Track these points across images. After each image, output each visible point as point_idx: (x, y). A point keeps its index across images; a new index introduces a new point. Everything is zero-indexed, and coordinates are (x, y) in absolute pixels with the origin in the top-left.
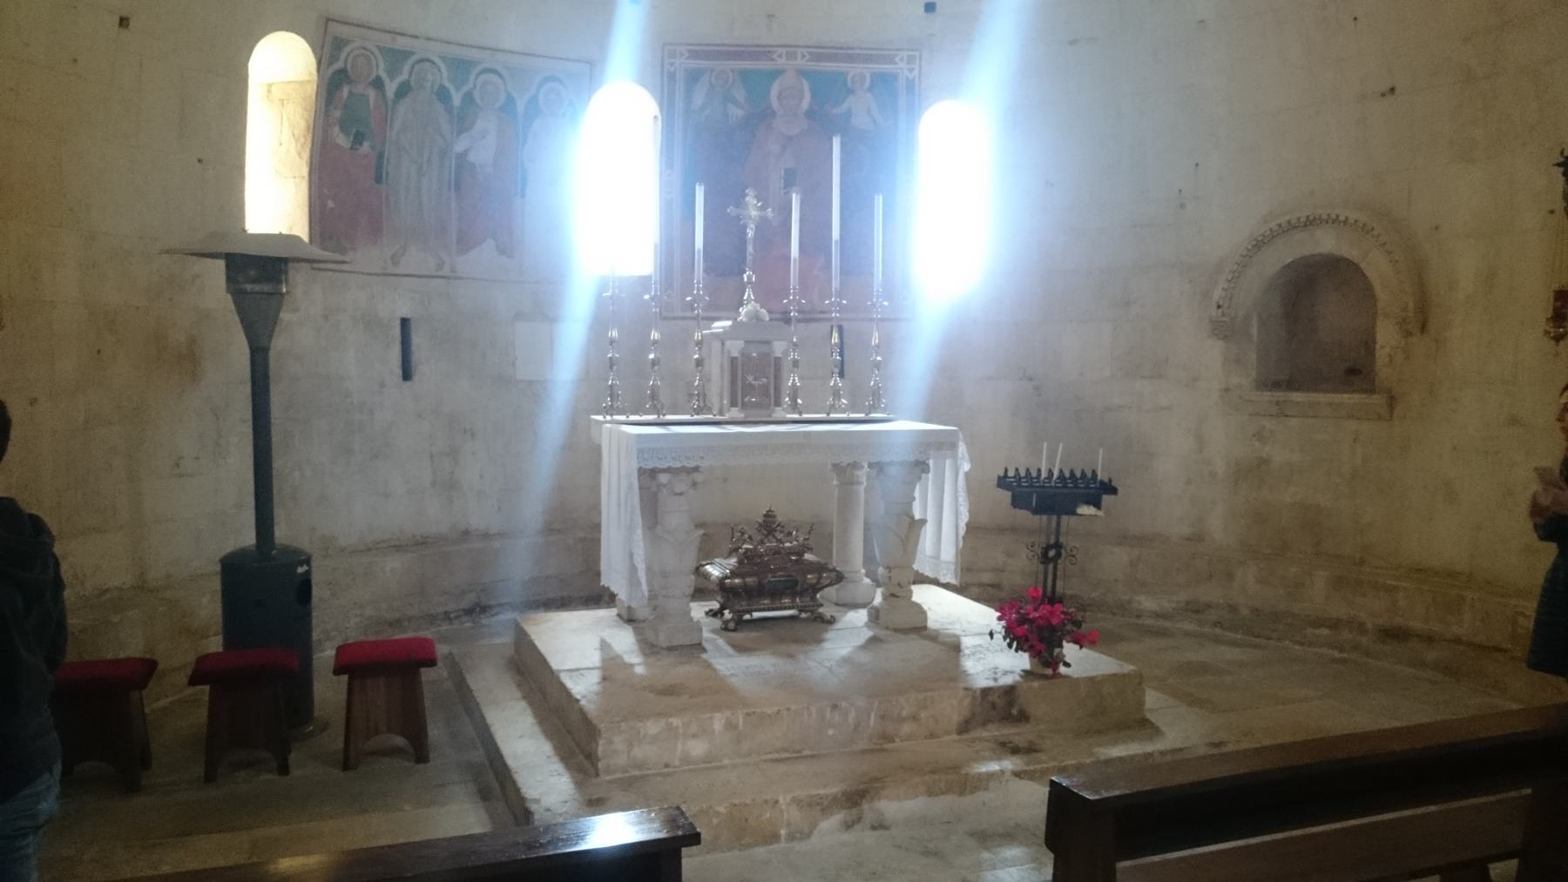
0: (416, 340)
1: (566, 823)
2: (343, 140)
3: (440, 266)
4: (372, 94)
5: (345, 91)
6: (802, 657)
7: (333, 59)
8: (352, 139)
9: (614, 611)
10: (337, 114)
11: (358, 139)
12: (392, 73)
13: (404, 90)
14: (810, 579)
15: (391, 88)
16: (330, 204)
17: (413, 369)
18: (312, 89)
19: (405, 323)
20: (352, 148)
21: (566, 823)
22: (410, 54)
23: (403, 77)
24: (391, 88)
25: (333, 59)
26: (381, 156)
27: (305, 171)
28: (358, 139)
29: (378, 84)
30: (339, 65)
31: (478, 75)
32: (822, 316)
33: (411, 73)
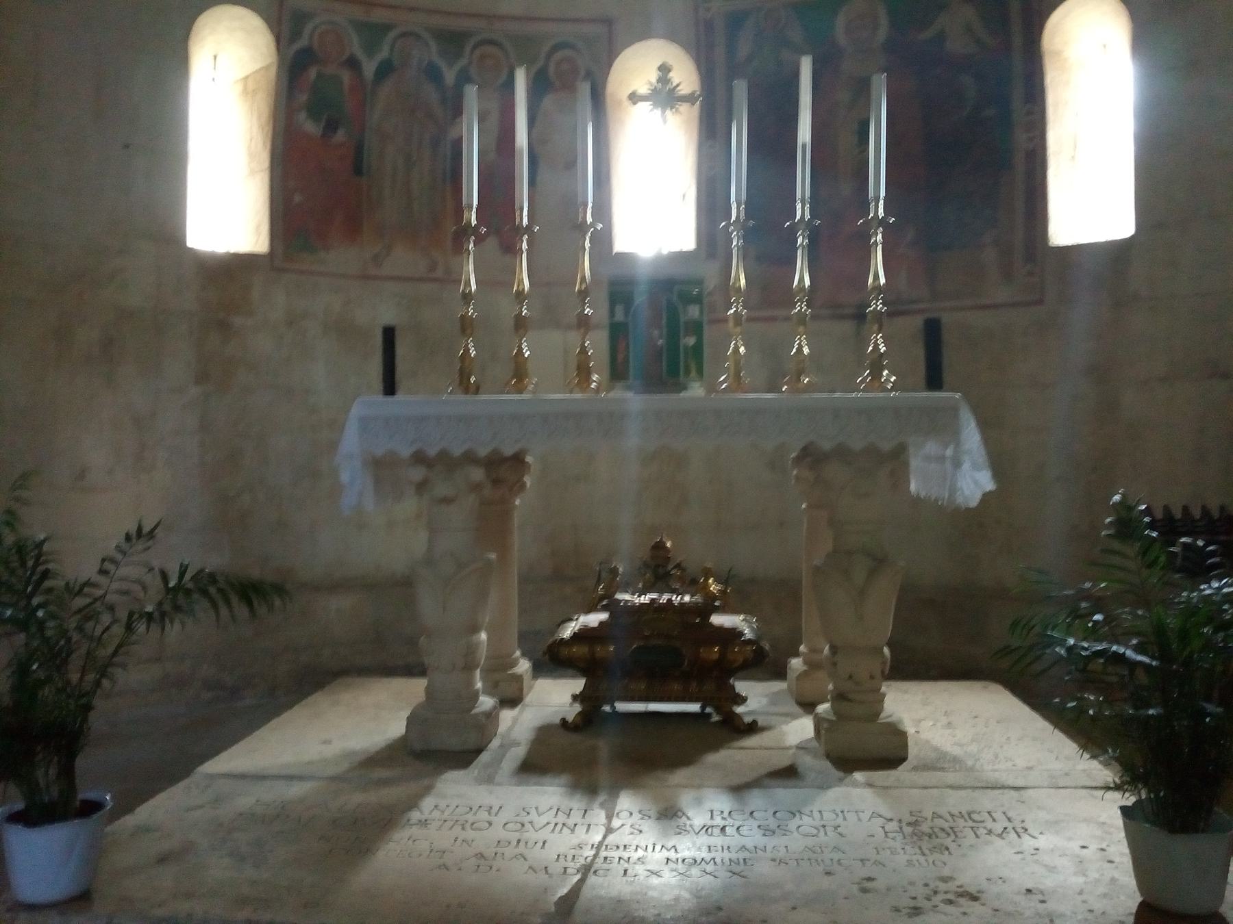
0: (401, 350)
1: (182, 563)
2: (311, 128)
3: (433, 267)
4: (346, 77)
5: (312, 73)
6: (1094, 747)
7: (296, 35)
8: (323, 124)
9: (778, 686)
10: (303, 98)
11: (331, 126)
12: (370, 49)
13: (385, 70)
14: (1208, 631)
15: (369, 68)
16: (297, 198)
17: (610, 129)
18: (273, 71)
19: (389, 335)
20: (324, 135)
21: (182, 563)
22: (386, 28)
23: (384, 54)
24: (369, 68)
25: (296, 35)
26: (359, 149)
27: (266, 163)
28: (331, 126)
29: (353, 64)
30: (302, 43)
31: (475, 47)
32: (915, 306)
33: (392, 50)
